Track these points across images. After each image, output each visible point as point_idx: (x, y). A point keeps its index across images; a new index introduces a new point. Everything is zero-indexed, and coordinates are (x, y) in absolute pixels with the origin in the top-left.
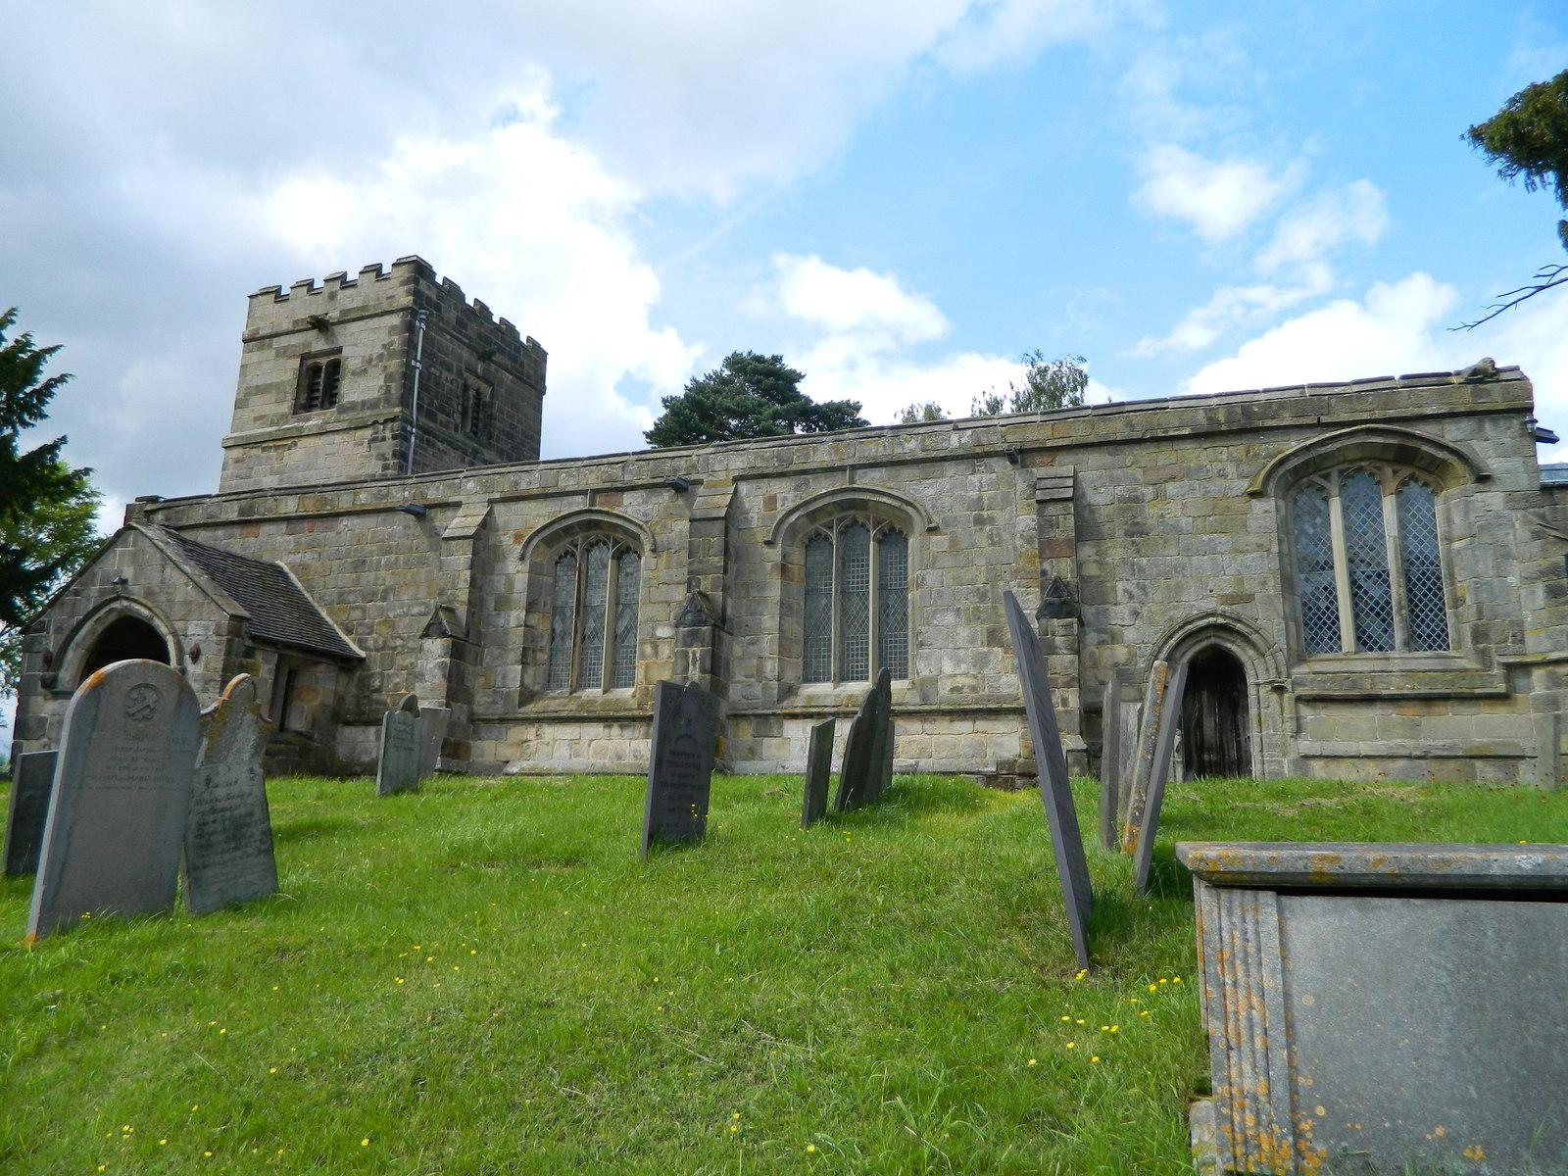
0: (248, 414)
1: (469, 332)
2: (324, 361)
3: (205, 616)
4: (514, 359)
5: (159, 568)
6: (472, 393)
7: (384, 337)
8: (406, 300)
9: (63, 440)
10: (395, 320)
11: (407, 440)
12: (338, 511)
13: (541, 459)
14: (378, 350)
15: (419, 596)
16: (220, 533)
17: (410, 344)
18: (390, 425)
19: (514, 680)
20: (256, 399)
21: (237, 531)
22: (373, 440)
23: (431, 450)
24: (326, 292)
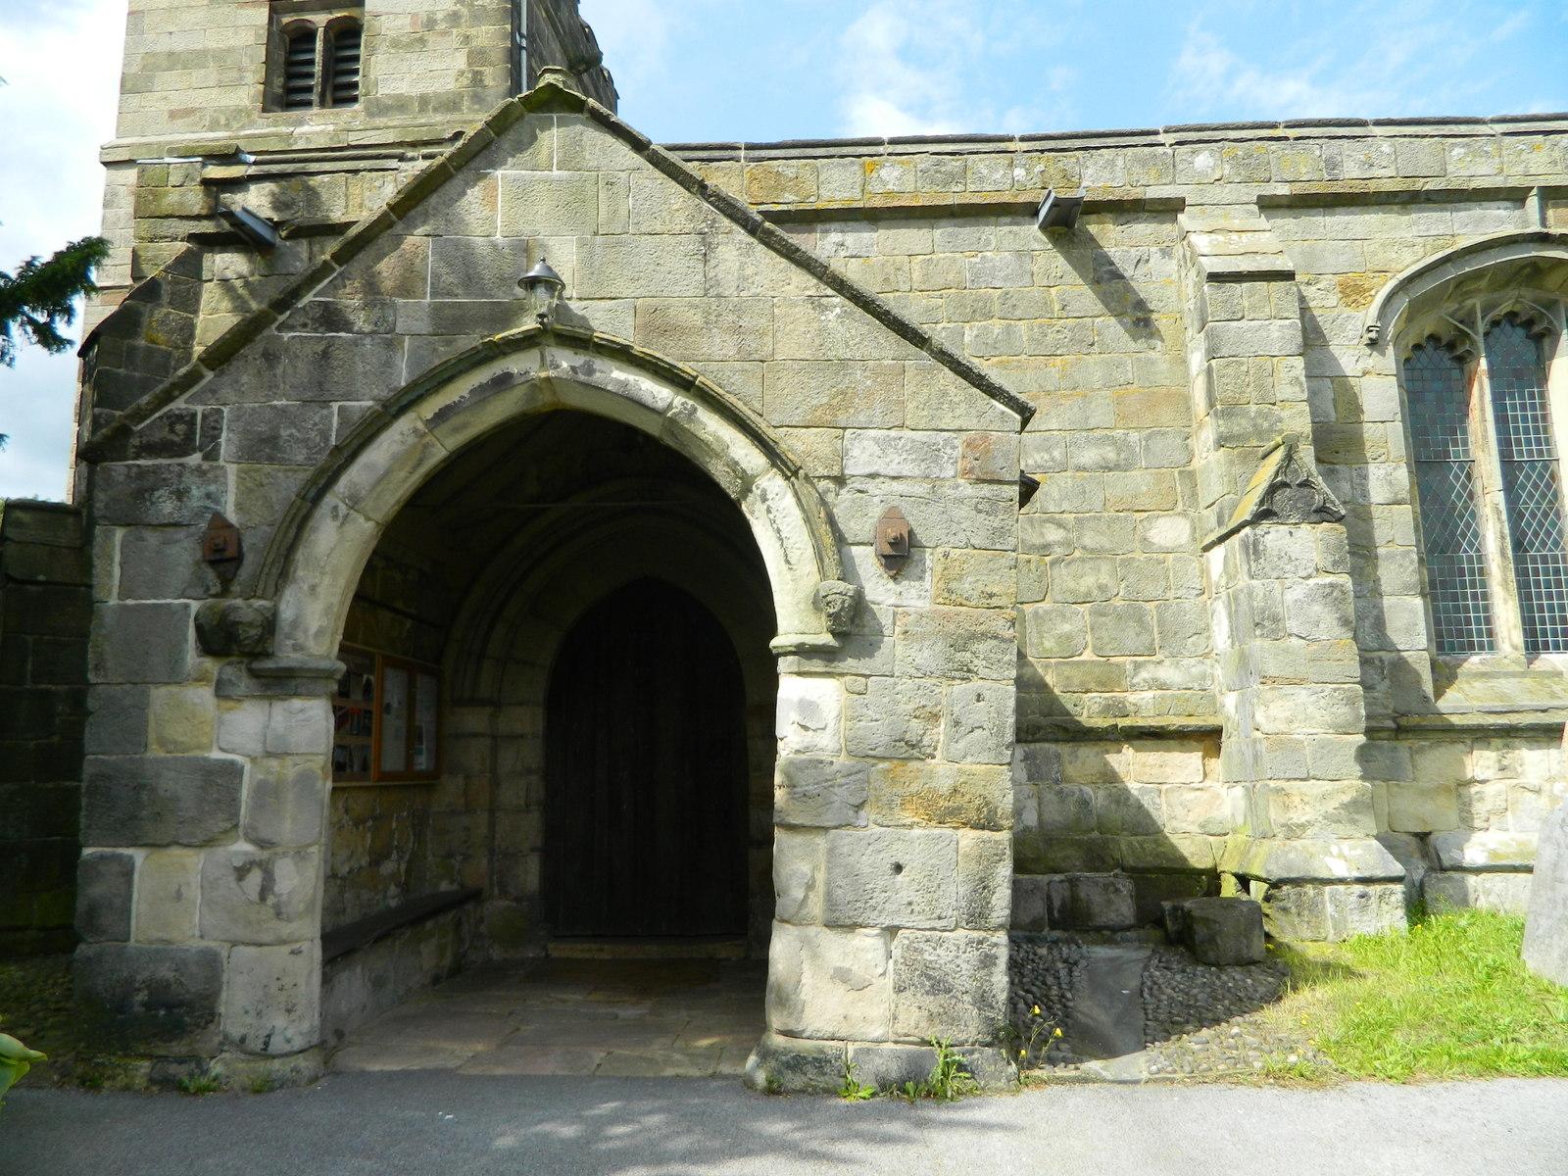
0: (155, 104)
3: (912, 413)
5: (692, 244)
12: (820, 205)
15: (1092, 423)
19: (1409, 630)
20: (167, 79)
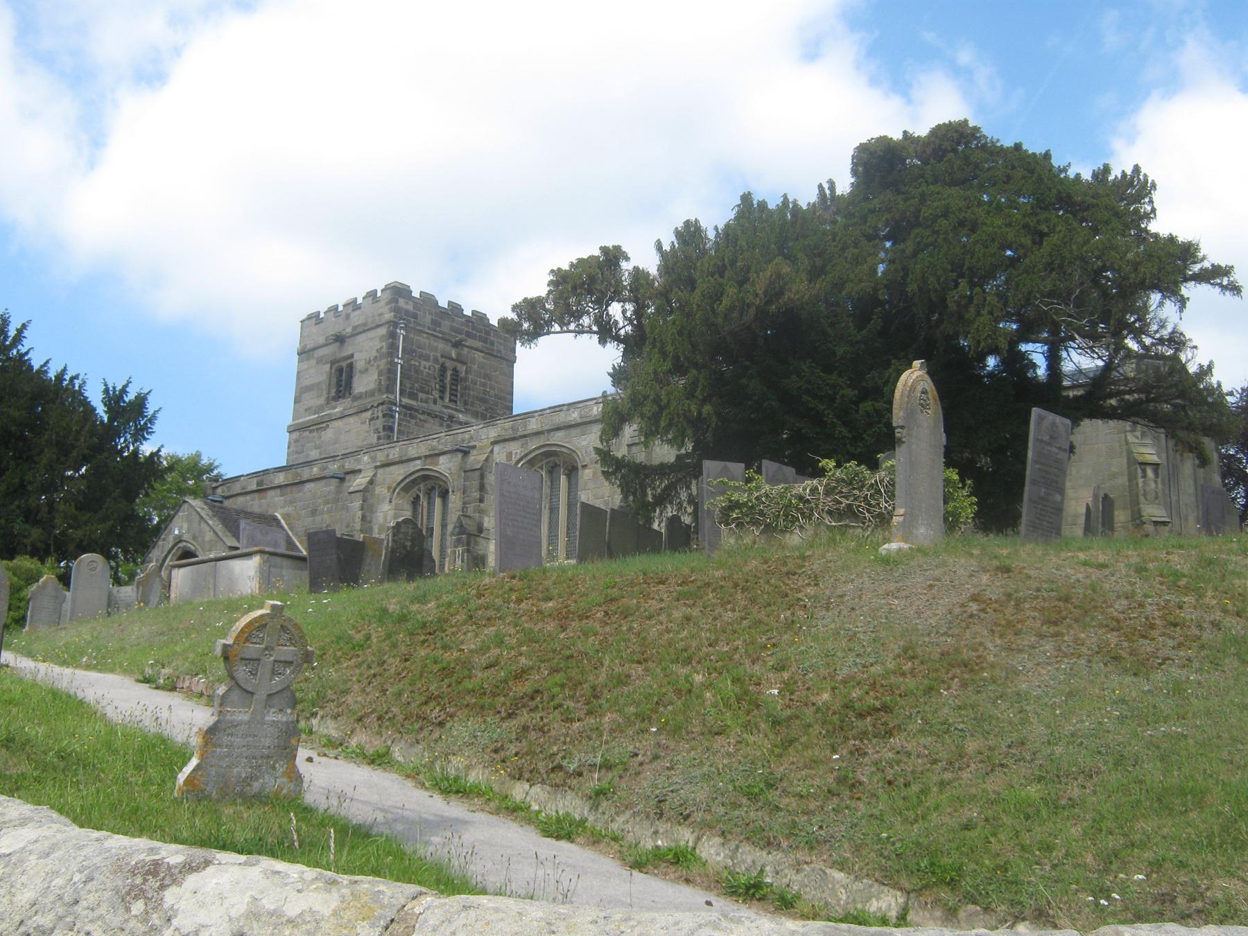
1: (443, 329)
2: (344, 364)
4: (485, 341)
6: (449, 373)
7: (377, 344)
8: (389, 316)
9: (162, 446)
10: (383, 331)
11: (393, 417)
13: (514, 413)
14: (374, 353)
16: (248, 497)
17: (393, 347)
18: (380, 408)
21: (256, 495)
22: (372, 419)
23: (413, 421)
24: (344, 314)
